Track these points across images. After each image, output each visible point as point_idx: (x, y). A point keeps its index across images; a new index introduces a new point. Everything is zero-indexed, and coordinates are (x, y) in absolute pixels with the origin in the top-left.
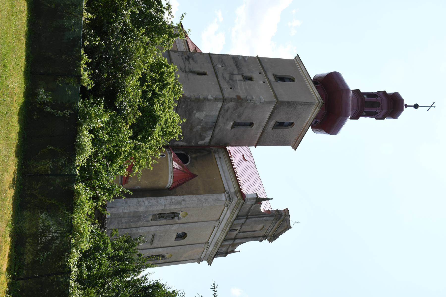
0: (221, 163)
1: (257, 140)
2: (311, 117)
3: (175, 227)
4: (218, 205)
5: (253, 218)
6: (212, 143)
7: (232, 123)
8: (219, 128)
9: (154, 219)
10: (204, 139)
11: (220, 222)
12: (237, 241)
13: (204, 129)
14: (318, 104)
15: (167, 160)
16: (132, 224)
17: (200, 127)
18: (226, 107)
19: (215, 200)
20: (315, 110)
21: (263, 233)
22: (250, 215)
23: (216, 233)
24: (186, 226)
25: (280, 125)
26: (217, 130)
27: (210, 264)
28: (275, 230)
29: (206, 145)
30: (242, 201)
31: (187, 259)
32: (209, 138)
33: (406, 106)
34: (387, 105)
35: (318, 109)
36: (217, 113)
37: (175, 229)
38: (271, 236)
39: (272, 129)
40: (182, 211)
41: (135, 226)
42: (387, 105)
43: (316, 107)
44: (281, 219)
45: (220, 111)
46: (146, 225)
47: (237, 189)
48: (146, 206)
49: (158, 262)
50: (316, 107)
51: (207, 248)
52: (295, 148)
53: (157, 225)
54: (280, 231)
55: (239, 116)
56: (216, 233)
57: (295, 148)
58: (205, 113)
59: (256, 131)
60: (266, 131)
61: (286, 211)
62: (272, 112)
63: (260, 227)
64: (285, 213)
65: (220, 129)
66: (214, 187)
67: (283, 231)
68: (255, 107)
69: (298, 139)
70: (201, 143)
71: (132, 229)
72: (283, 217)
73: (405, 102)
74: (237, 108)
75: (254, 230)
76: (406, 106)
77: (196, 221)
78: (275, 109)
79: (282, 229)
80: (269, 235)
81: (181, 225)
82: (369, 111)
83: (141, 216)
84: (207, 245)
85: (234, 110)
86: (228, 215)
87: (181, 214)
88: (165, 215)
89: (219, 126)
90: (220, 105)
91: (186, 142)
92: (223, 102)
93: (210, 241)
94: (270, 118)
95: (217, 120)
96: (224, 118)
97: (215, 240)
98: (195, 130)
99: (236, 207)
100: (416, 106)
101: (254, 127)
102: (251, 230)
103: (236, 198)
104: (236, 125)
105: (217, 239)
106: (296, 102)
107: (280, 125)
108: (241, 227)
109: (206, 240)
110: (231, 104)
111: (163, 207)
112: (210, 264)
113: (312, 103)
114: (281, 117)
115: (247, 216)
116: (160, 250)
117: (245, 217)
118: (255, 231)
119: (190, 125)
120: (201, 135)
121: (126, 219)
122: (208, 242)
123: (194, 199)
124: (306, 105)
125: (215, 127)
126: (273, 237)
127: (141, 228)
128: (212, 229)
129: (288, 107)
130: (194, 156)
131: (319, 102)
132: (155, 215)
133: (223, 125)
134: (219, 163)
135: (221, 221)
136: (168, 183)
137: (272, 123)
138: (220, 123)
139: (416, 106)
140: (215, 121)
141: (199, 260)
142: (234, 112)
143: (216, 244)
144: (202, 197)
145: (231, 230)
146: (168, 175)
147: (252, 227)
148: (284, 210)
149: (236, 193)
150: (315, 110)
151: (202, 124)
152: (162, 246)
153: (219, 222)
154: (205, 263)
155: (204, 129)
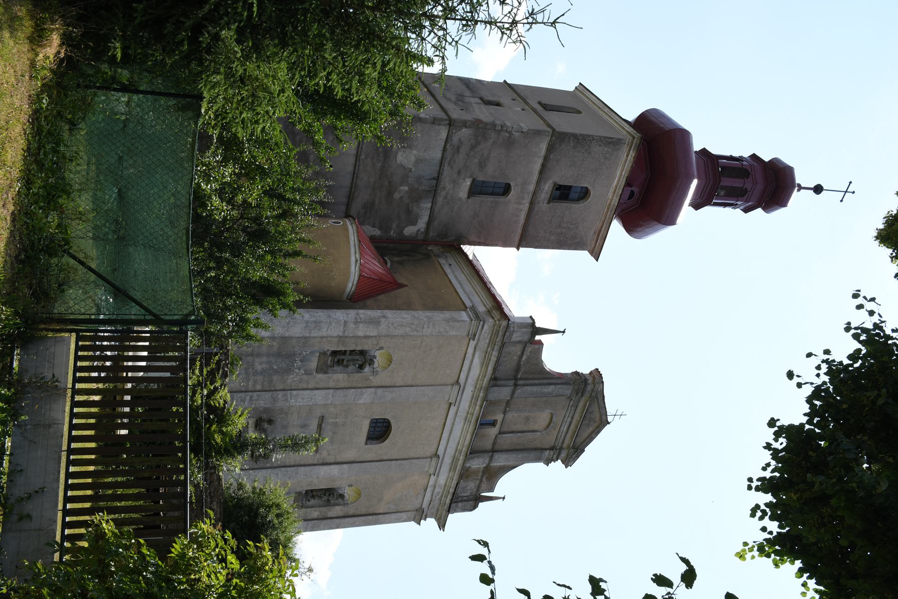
0: (453, 271)
1: (519, 231)
2: (621, 175)
3: (367, 397)
4: (454, 333)
5: (527, 385)
6: (431, 234)
7: (468, 182)
8: (443, 193)
9: (322, 369)
10: (414, 223)
11: (462, 391)
12: (500, 460)
13: (416, 196)
14: (632, 142)
15: (347, 230)
16: (275, 378)
17: (406, 188)
18: (455, 140)
19: (448, 321)
20: (627, 156)
21: (550, 439)
22: (521, 379)
23: (453, 424)
24: (389, 395)
25: (563, 193)
26: (440, 200)
27: (442, 525)
28: (577, 433)
29: (421, 237)
30: (504, 323)
31: (393, 508)
32: (425, 219)
33: (800, 188)
34: (763, 184)
35: (632, 154)
36: (439, 155)
37: (366, 404)
38: (568, 447)
39: (548, 203)
40: (381, 348)
41: (281, 387)
42: (763, 184)
43: (629, 150)
44: (587, 395)
45: (445, 150)
46: (305, 386)
47: (490, 304)
48: (307, 322)
49: (330, 514)
50: (629, 150)
51: (436, 473)
52: (596, 255)
53: (329, 388)
54: (586, 434)
55: (482, 165)
56: (453, 424)
57: (596, 255)
58: (415, 152)
59: (515, 206)
60: (536, 209)
61: (596, 376)
62: (546, 159)
63: (542, 418)
64: (594, 377)
65: (446, 197)
66: (443, 301)
67: (593, 432)
68: (510, 143)
69: (600, 230)
70: (409, 231)
71: (275, 394)
72: (589, 388)
73: (798, 180)
74: (478, 143)
75: (532, 428)
76: (800, 188)
77: (410, 382)
78: (550, 149)
79: (591, 429)
80: (565, 445)
81: (380, 391)
82: (730, 184)
83: (294, 354)
84: (434, 460)
85: (473, 148)
86: (475, 371)
87: (380, 359)
88: (346, 358)
89: (444, 188)
90: (444, 134)
91: (380, 229)
92: (450, 125)
93: (440, 452)
94: (541, 172)
95: (440, 173)
96: (452, 167)
97: (451, 451)
98: (397, 196)
99: (492, 343)
100: (818, 189)
101: (513, 193)
102: (526, 428)
103: (491, 320)
104: (477, 189)
105: (454, 446)
106: (589, 136)
107: (563, 193)
108: (505, 413)
109: (432, 450)
110: (465, 133)
111: (342, 329)
112: (442, 525)
113: (620, 140)
114: (563, 175)
115: (516, 379)
116: (335, 470)
117: (512, 382)
118: (533, 431)
119: (386, 183)
120: (409, 212)
121: (264, 359)
122: (436, 455)
123: (405, 316)
124: (609, 143)
125: (435, 191)
126: (569, 452)
127: (295, 392)
128: (443, 413)
129: (574, 147)
130: (396, 259)
131: (634, 138)
132: (324, 353)
133: (452, 185)
134: (448, 270)
135: (462, 383)
136: (348, 278)
137: (547, 187)
138: (446, 182)
139: (818, 189)
140: (436, 175)
141: (419, 516)
142: (472, 153)
143: (455, 460)
144: (423, 315)
145: (484, 423)
146: (350, 258)
147: (527, 419)
148: (591, 373)
149: (489, 312)
150: (627, 156)
151: (410, 180)
152: (339, 460)
153: (458, 387)
154: (430, 523)
155: (416, 196)
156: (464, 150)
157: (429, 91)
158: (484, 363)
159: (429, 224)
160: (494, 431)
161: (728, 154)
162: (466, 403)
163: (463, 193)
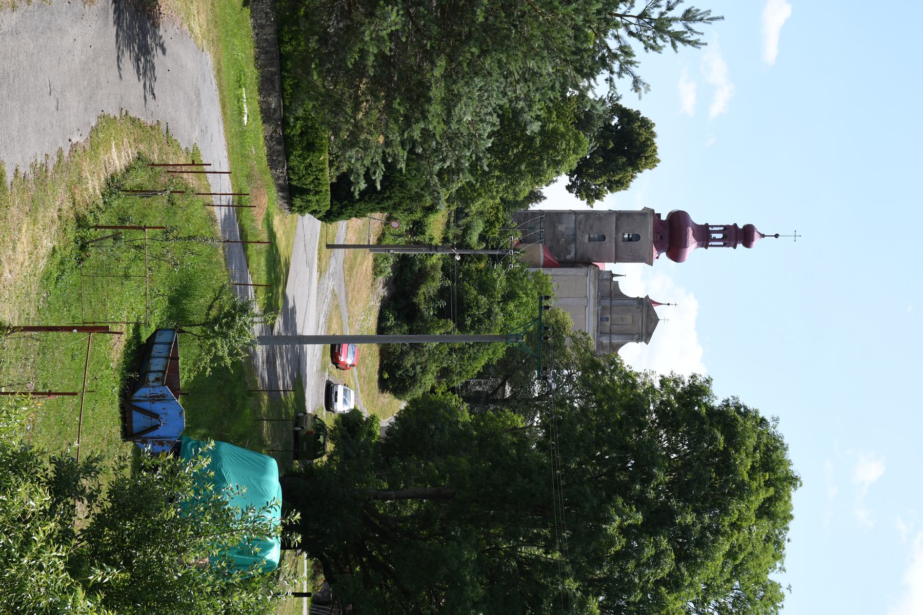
13: (568, 243)
62: (616, 223)
63: (629, 319)
78: (617, 219)
90: (574, 218)
120: (566, 249)
138: (579, 236)
155: (568, 243)
156: (583, 222)
157: (81, 329)
158: (595, 288)
159: (575, 254)
160: (608, 323)
161: (568, 209)
162: (592, 307)
163: (586, 240)
